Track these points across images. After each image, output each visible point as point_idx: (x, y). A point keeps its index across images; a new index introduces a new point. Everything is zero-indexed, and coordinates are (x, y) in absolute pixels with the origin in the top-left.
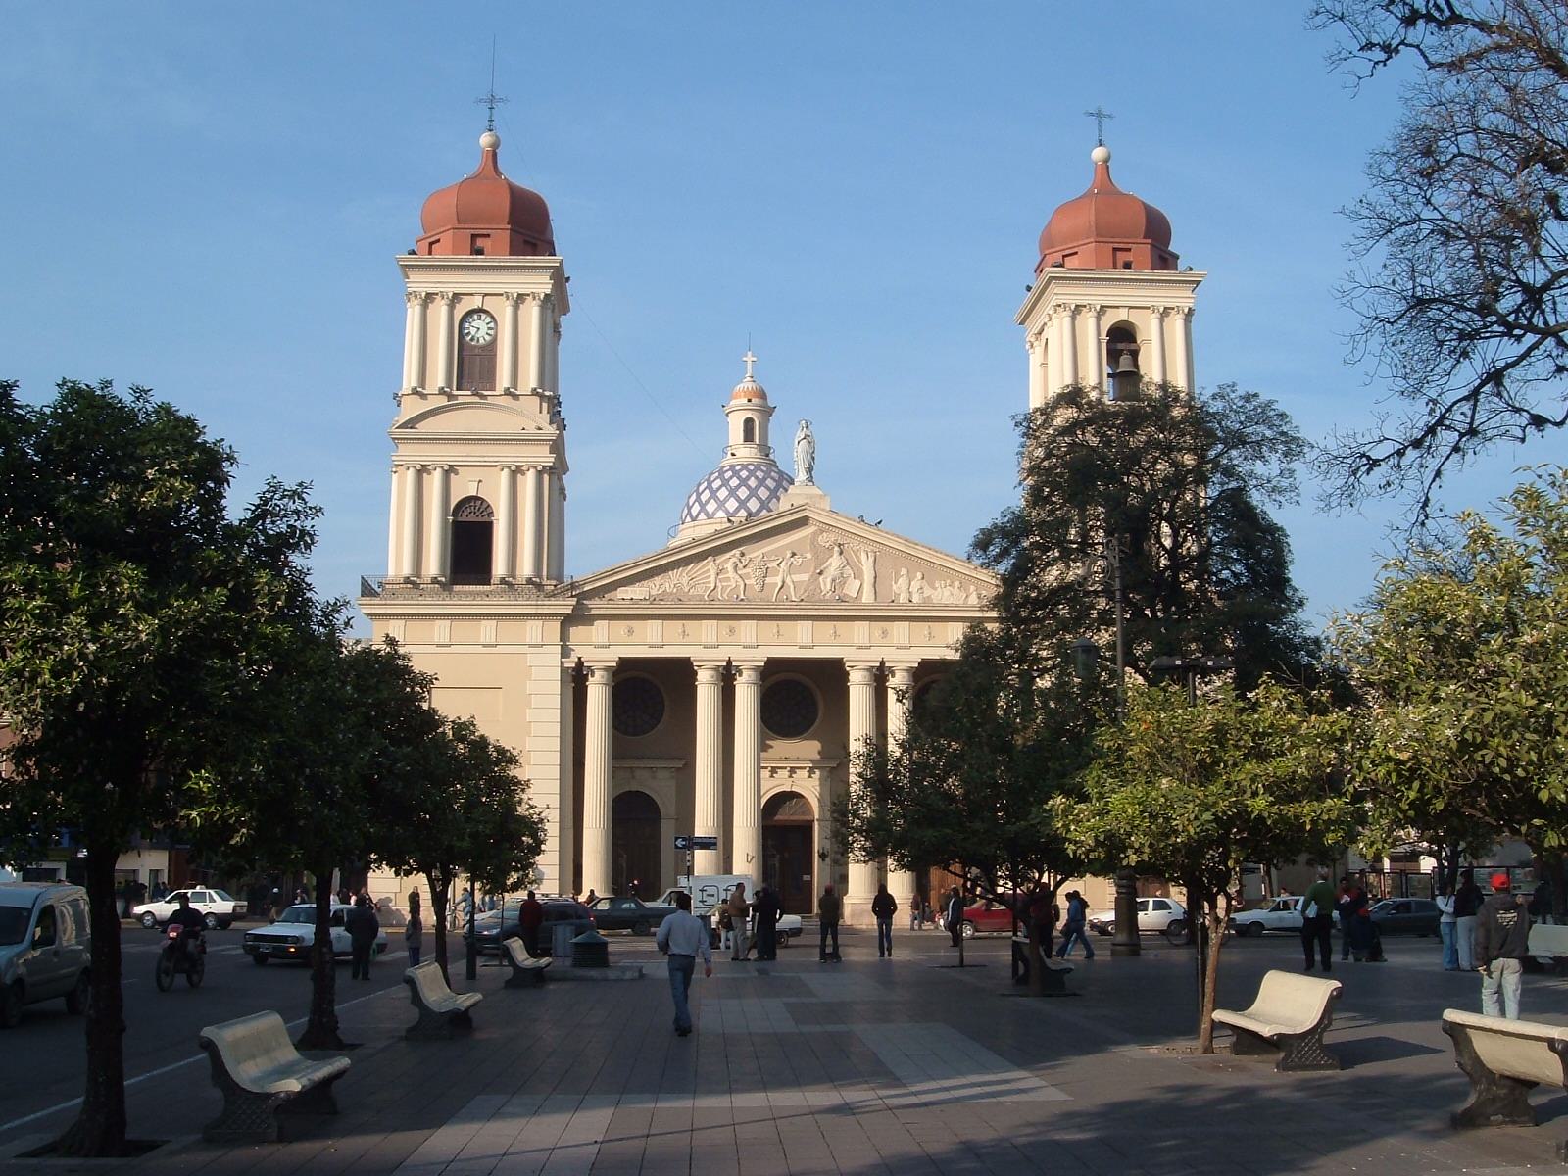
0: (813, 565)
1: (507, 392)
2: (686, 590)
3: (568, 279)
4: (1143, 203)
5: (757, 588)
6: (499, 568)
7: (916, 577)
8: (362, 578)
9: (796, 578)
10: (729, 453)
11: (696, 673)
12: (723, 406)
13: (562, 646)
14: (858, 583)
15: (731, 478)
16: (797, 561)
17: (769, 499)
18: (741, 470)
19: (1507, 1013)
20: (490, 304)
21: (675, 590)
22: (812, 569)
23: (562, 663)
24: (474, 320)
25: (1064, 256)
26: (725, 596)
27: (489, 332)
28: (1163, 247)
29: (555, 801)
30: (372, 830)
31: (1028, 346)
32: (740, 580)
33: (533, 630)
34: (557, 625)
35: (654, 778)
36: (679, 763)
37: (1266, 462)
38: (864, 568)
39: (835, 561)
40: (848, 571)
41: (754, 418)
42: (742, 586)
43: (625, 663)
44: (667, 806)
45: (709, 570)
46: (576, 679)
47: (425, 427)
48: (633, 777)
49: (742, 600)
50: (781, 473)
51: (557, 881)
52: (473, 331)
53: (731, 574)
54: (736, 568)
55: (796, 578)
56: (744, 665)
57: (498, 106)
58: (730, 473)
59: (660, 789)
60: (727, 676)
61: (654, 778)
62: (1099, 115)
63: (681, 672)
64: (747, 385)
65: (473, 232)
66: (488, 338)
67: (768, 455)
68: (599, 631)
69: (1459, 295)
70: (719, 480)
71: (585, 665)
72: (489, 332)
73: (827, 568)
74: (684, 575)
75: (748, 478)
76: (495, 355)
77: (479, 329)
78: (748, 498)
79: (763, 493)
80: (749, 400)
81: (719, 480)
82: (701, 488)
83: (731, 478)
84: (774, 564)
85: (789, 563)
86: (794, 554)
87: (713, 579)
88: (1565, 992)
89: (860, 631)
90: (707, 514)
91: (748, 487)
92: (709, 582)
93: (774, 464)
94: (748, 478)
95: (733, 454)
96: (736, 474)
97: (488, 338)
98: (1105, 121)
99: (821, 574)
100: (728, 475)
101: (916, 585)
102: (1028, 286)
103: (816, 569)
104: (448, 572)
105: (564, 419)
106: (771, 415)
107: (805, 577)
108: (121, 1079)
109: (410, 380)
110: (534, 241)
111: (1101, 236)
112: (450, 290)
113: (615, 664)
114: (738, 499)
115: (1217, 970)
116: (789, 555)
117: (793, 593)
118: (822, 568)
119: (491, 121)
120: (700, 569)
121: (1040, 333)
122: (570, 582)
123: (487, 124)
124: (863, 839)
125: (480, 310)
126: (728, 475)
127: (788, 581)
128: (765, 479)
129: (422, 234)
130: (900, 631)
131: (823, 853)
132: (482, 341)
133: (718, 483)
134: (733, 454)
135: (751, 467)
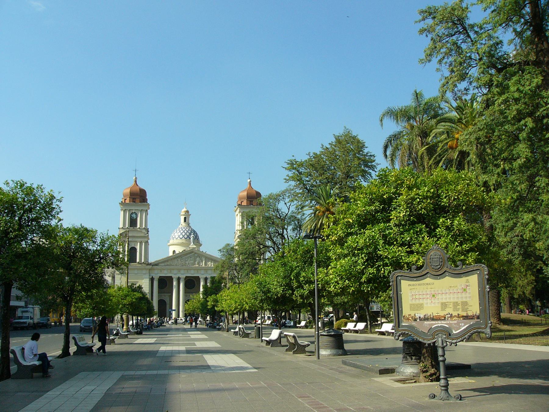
6: (138, 261)
9: (191, 262)
16: (191, 259)
17: (189, 235)
19: (390, 367)
33: (144, 272)
34: (148, 271)
36: (170, 294)
37: (497, 91)
39: (198, 259)
40: (200, 261)
46: (152, 280)
50: (192, 229)
52: (133, 216)
54: (180, 260)
55: (191, 262)
59: (166, 298)
60: (179, 279)
63: (171, 279)
64: (185, 210)
68: (156, 272)
75: (185, 231)
77: (134, 216)
78: (185, 235)
79: (188, 234)
88: (548, 386)
90: (180, 238)
91: (185, 233)
93: (190, 227)
94: (185, 231)
96: (182, 230)
98: (250, 175)
100: (180, 230)
101: (212, 264)
107: (193, 262)
108: (9, 367)
109: (121, 226)
112: (129, 209)
114: (182, 235)
124: (370, 269)
128: (188, 231)
129: (123, 197)
135: (185, 228)
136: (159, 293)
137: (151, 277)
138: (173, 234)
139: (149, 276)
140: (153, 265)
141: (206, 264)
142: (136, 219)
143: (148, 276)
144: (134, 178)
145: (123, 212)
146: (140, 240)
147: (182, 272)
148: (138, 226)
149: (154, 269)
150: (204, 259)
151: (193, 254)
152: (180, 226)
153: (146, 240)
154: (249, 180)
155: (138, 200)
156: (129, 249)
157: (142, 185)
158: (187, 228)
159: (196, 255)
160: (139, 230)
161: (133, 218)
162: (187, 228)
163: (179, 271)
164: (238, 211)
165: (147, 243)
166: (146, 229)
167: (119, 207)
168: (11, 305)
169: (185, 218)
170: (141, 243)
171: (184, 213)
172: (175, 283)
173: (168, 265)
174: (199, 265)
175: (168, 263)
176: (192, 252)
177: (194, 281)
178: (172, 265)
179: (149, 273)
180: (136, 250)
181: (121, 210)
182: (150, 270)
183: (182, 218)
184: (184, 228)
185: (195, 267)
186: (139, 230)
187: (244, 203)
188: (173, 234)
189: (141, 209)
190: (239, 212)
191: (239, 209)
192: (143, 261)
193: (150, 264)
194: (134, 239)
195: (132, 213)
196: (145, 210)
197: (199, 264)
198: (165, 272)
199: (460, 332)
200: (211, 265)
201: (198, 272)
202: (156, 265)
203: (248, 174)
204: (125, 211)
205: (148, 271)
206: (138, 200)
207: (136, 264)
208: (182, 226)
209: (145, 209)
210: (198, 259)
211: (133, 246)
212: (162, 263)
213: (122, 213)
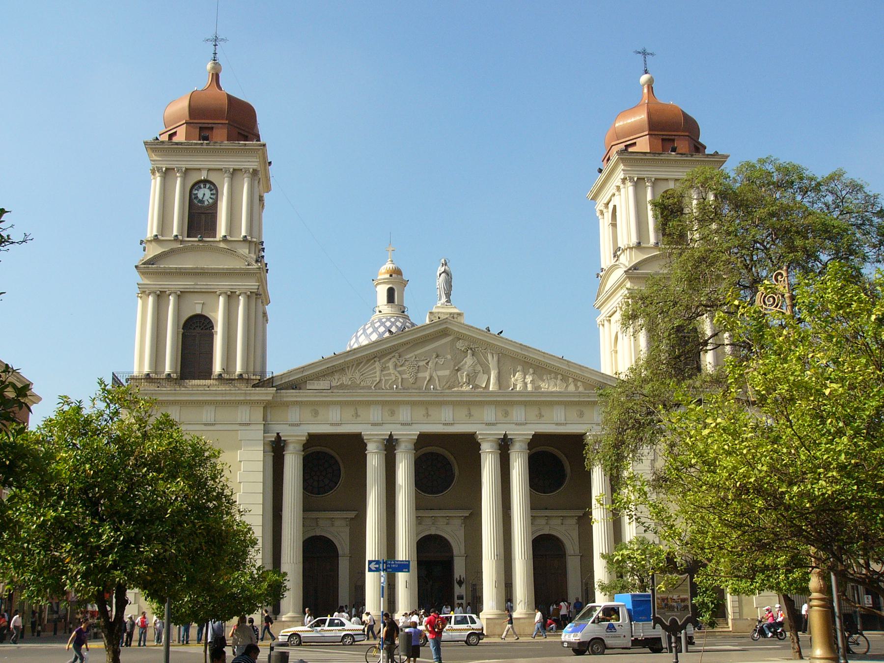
0: (453, 363)
1: (225, 239)
2: (358, 382)
3: (270, 163)
4: (682, 111)
5: (411, 380)
6: (217, 368)
7: (529, 372)
8: (113, 374)
9: (440, 373)
10: (377, 312)
11: (366, 445)
12: (373, 280)
13: (264, 425)
14: (486, 377)
15: (380, 326)
16: (441, 361)
18: (386, 322)
20: (213, 177)
21: (350, 383)
22: (452, 366)
23: (264, 437)
24: (205, 187)
25: (625, 146)
26: (387, 386)
27: (212, 196)
28: (695, 138)
29: (258, 510)
30: (92, 564)
31: (598, 214)
32: (398, 375)
33: (243, 414)
35: (333, 525)
36: (352, 515)
38: (490, 366)
39: (469, 361)
40: (479, 368)
41: (394, 287)
42: (400, 380)
43: (313, 439)
44: (343, 546)
45: (375, 367)
47: (163, 265)
48: (317, 525)
49: (401, 389)
51: (262, 473)
52: (200, 196)
53: (392, 371)
54: (396, 366)
55: (440, 373)
56: (403, 438)
57: (219, 43)
58: (378, 324)
61: (333, 525)
62: (644, 53)
64: (389, 266)
65: (201, 125)
66: (211, 201)
67: (403, 312)
68: (294, 415)
69: (709, 307)
70: (371, 328)
71: (282, 439)
72: (212, 196)
73: (463, 365)
74: (357, 371)
75: (391, 326)
76: (216, 213)
77: (204, 194)
80: (391, 276)
81: (371, 328)
82: (359, 334)
83: (380, 326)
84: (424, 363)
85: (435, 362)
86: (437, 356)
87: (378, 374)
89: (489, 414)
92: (376, 377)
93: (407, 318)
95: (380, 312)
96: (383, 324)
97: (211, 201)
98: (648, 58)
99: (458, 370)
100: (377, 325)
101: (529, 379)
102: (600, 169)
103: (455, 367)
104: (179, 370)
105: (266, 264)
106: (405, 286)
109: (152, 230)
110: (246, 134)
111: (653, 130)
112: (184, 166)
113: (305, 438)
115: (315, 619)
116: (434, 356)
117: (438, 385)
118: (459, 366)
119: (215, 54)
120: (367, 368)
121: (608, 204)
122: (271, 376)
123: (213, 56)
125: (205, 181)
126: (377, 325)
127: (434, 374)
130: (518, 414)
131: (460, 580)
132: (206, 203)
133: (371, 330)
134: (380, 312)
135: (393, 320)
136: (305, 510)
137: (272, 437)
138: (354, 340)
139: (265, 431)
140: (279, 388)
141: (501, 379)
142: (214, 206)
143: (257, 432)
144: (209, 66)
145: (159, 179)
146: (226, 284)
147: (404, 414)
148: (222, 230)
149: (286, 405)
150: (492, 361)
151: (449, 339)
152: (376, 316)
153: (252, 284)
154: (644, 78)
155: (220, 134)
156: (298, 633)
157: (232, 86)
158: (396, 321)
159: (460, 345)
160: (222, 245)
161: (202, 201)
162: (396, 321)
163: (393, 413)
164: (619, 174)
165: (259, 297)
166: (250, 242)
167: (145, 160)
168: (224, 649)
169: (391, 293)
170: (231, 297)
171: (388, 276)
172: (374, 462)
173: (342, 387)
174: (476, 387)
175: (345, 380)
176: (444, 333)
177: (448, 463)
178: (363, 388)
179: (265, 419)
180: (212, 327)
181: (153, 172)
182: (268, 406)
183: (382, 292)
184: (388, 320)
185: (463, 393)
186: (222, 245)
187: (643, 144)
188: (354, 340)
189: (232, 166)
190: (624, 180)
191: (621, 167)
192: (239, 369)
193: (270, 382)
194: (203, 283)
195: (197, 185)
196: (247, 170)
197: (471, 379)
198: (334, 414)
199: (485, 660)
200: (526, 384)
201: (470, 415)
202: (295, 385)
203: (641, 57)
204: (167, 174)
205: (258, 414)
206: (220, 134)
207: (208, 382)
208: (381, 316)
209: (252, 163)
210: (469, 361)
211: (198, 311)
212: (318, 376)
213: (156, 183)
